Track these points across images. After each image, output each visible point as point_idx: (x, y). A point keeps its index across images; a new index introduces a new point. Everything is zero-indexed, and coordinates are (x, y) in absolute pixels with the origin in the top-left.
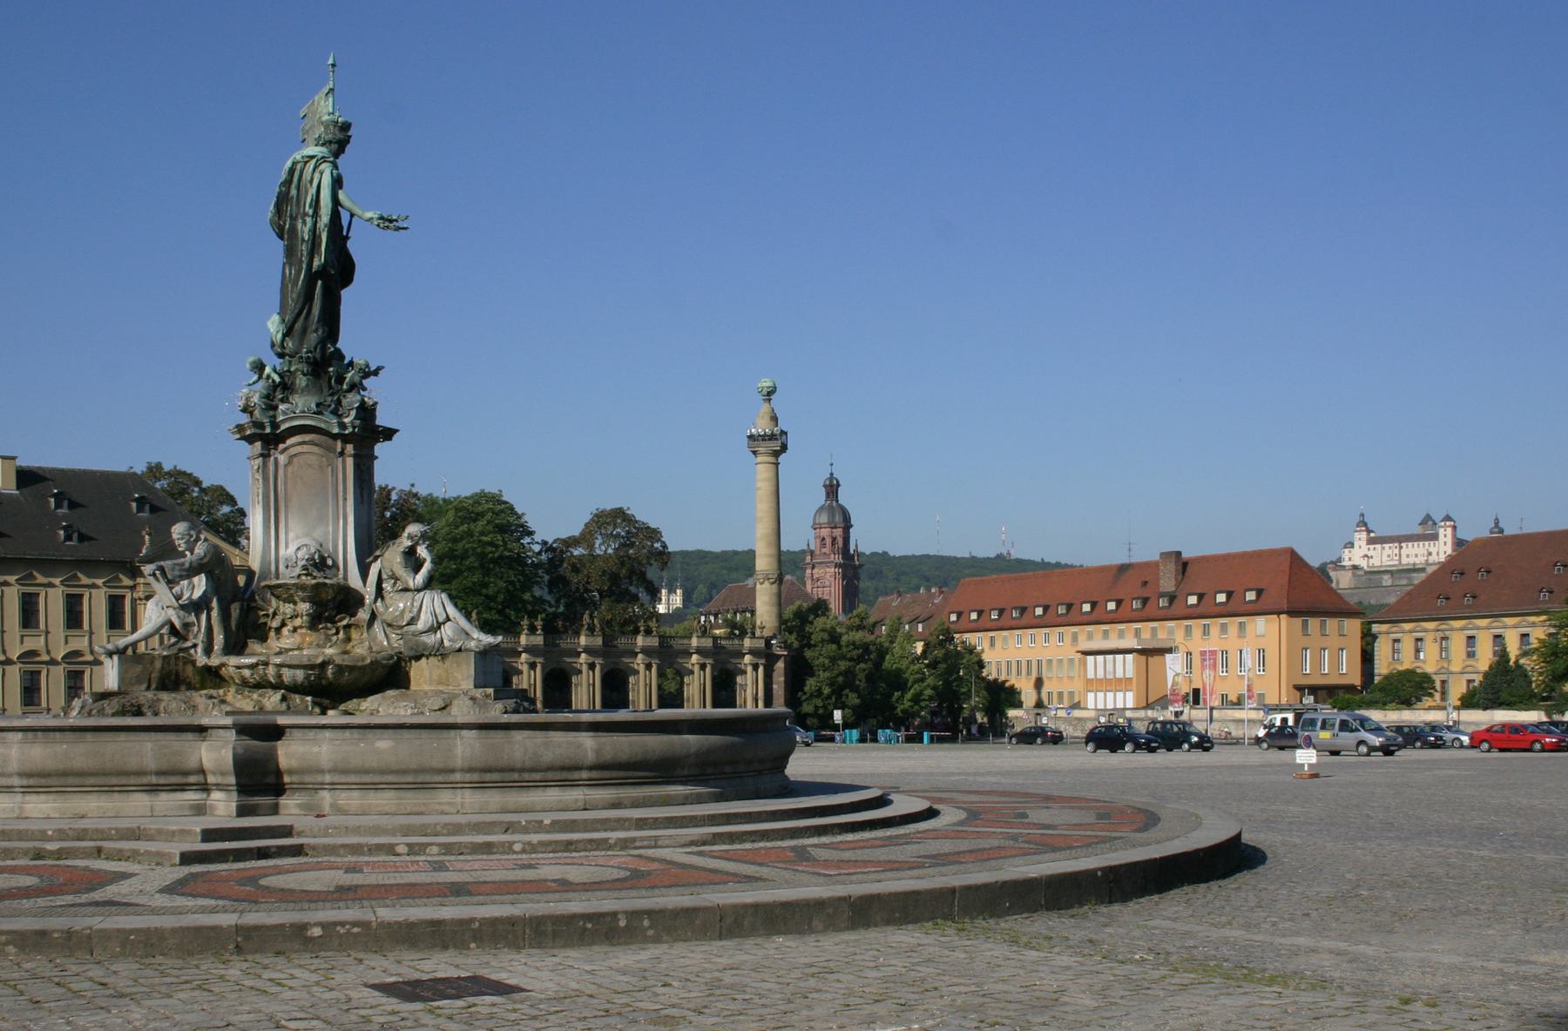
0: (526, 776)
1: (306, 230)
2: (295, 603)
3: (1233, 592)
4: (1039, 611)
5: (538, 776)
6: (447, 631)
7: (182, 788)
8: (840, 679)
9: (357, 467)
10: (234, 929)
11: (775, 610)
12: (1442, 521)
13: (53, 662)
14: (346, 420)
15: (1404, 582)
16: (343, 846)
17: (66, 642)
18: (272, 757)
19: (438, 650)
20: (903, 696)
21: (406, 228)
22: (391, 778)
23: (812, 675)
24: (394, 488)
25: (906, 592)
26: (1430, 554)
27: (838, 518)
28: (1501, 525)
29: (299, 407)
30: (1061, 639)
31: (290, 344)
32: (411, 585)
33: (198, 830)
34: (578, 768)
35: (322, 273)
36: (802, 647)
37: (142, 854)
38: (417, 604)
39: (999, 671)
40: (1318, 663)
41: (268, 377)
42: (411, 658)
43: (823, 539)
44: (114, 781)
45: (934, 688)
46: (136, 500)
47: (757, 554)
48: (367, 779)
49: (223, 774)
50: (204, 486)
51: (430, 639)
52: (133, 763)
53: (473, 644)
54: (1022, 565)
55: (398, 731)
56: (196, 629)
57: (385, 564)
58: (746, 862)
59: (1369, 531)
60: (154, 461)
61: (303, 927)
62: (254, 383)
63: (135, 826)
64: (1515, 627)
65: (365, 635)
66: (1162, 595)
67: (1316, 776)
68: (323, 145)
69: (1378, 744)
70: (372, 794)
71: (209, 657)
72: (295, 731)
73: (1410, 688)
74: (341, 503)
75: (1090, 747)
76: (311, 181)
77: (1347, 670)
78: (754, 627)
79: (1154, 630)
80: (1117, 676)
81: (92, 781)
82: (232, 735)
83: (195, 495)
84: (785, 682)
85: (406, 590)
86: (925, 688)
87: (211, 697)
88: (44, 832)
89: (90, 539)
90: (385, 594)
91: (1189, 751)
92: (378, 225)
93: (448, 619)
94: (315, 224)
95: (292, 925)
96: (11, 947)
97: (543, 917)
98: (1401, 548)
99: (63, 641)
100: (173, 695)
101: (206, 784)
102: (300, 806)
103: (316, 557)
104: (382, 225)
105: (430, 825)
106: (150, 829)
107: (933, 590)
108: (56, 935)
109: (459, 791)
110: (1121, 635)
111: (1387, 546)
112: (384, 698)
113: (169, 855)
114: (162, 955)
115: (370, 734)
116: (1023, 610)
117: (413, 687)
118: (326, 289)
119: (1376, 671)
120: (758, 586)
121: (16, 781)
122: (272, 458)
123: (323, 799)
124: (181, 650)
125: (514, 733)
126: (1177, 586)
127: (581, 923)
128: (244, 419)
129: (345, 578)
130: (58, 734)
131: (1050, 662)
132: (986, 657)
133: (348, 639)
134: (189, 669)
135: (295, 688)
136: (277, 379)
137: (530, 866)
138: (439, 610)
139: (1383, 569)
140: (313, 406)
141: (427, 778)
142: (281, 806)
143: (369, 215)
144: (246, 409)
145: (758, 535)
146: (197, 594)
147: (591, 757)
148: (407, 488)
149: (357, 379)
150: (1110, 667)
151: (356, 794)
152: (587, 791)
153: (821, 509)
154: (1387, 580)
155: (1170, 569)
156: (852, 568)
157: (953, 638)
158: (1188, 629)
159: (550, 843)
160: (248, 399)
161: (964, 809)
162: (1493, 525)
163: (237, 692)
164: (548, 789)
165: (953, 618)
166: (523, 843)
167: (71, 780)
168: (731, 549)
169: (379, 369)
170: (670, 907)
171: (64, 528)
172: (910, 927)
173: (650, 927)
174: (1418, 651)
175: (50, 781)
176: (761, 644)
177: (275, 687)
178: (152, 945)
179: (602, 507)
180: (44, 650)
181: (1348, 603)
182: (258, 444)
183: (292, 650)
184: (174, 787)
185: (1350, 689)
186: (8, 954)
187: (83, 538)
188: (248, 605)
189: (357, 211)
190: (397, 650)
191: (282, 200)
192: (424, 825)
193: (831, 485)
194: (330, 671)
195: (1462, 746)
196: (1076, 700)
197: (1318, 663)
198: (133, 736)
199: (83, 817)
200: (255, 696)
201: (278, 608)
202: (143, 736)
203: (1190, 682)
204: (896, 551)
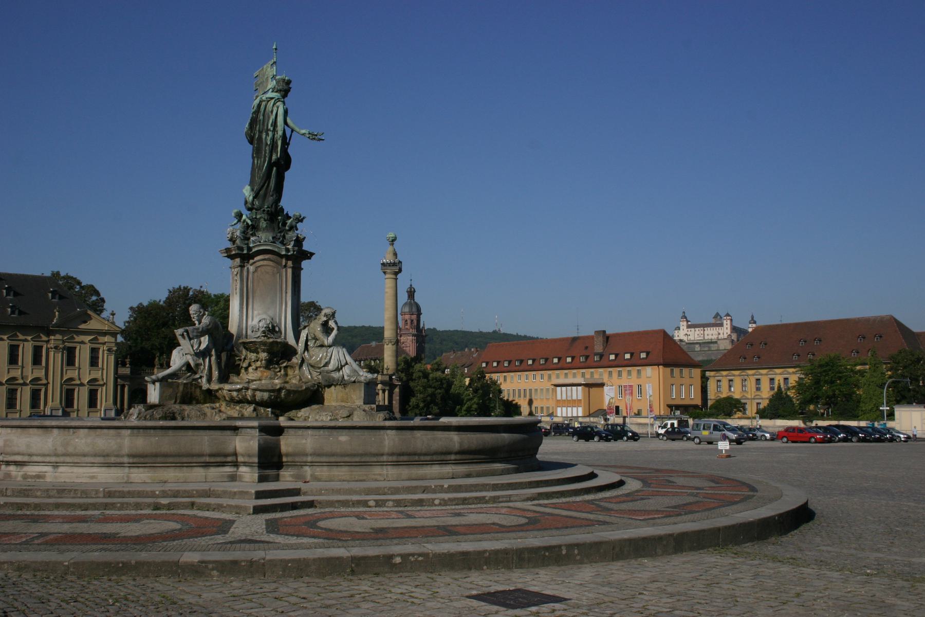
0: (422, 458)
1: (269, 138)
2: (258, 353)
3: (649, 352)
4: (530, 362)
5: (428, 458)
6: (346, 371)
7: (223, 464)
8: (429, 398)
9: (293, 273)
10: (350, 559)
11: (394, 359)
13: (82, 385)
14: (290, 247)
15: (706, 349)
16: (338, 501)
17: (8, 372)
18: (278, 446)
19: (342, 382)
20: (461, 409)
21: (323, 140)
22: (347, 459)
23: (414, 396)
24: (191, 288)
25: (458, 351)
26: (719, 334)
27: (414, 309)
28: (755, 319)
29: (262, 239)
30: (542, 377)
31: (257, 203)
32: (326, 343)
33: (253, 491)
34: (449, 453)
35: (277, 163)
36: (408, 381)
37: (225, 507)
38: (329, 355)
39: (509, 395)
40: (679, 392)
41: (244, 221)
42: (325, 386)
43: (406, 321)
44: (185, 460)
45: (478, 404)
46: (51, 292)
47: (385, 328)
48: (332, 459)
49: (249, 456)
50: (83, 285)
51: (336, 375)
52: (196, 449)
53: (362, 379)
54: (507, 337)
55: (351, 430)
56: (202, 367)
57: (311, 331)
58: (584, 512)
59: (688, 321)
60: (56, 270)
61: (391, 557)
62: (235, 224)
63: (207, 488)
64: (780, 374)
65: (297, 372)
66: (596, 354)
67: (729, 456)
68: (276, 92)
69: (734, 438)
70: (335, 469)
71: (210, 384)
72: (290, 430)
73: (731, 406)
74: (284, 294)
75: (575, 438)
76: (272, 112)
77: (694, 397)
78: (383, 369)
79: (592, 373)
81: (171, 460)
82: (256, 433)
83: (77, 290)
84: (400, 399)
85: (322, 346)
86: (473, 404)
87: (213, 408)
88: (153, 492)
89: (25, 313)
90: (310, 349)
91: (627, 441)
92: (309, 138)
93: (347, 364)
94: (274, 135)
95: (384, 556)
96: (215, 572)
97: (523, 548)
98: (704, 330)
99: (6, 372)
100: (191, 407)
101: (237, 462)
102: (292, 476)
103: (270, 326)
104: (311, 138)
105: (381, 488)
106: (218, 491)
107: (473, 350)
108: (243, 564)
109: (384, 467)
110: (574, 376)
111: (697, 329)
112: (311, 409)
113: (245, 508)
114: (307, 576)
115: (335, 432)
116: (521, 361)
117: (326, 403)
118: (278, 171)
119: (709, 397)
120: (385, 346)
121: (126, 460)
122: (246, 268)
123: (306, 471)
124: (194, 380)
125: (415, 432)
126: (604, 349)
127: (543, 553)
128: (229, 245)
129: (285, 338)
130: (152, 431)
131: (536, 390)
132: (503, 387)
133: (286, 375)
134: (198, 391)
135: (263, 404)
136: (250, 223)
137: (459, 515)
138: (342, 358)
140: (271, 238)
142: (281, 476)
143: (303, 131)
144: (232, 240)
145: (386, 318)
146: (203, 347)
147: (457, 447)
148: (198, 288)
149: (294, 223)
150: (569, 394)
151: (325, 469)
152: (454, 467)
153: (406, 304)
154: (697, 348)
156: (422, 336)
157: (485, 376)
159: (455, 499)
160: (233, 233)
161: (639, 479)
162: (751, 319)
163: (227, 405)
164: (433, 466)
165: (484, 365)
166: (440, 500)
167: (159, 459)
168: (353, 325)
169: (304, 218)
170: (588, 542)
171: (11, 307)
172: (701, 551)
173: (578, 554)
174: (730, 387)
175: (146, 460)
176: (387, 378)
177: (249, 403)
178: (301, 569)
179: (154, 299)
180: (77, 378)
181: (693, 360)
182: (238, 260)
183: (255, 380)
184: (218, 464)
185: (696, 407)
186: (213, 577)
187: (21, 313)
188: (230, 353)
189: (297, 129)
190: (317, 381)
191: (253, 122)
192: (377, 488)
193: (411, 291)
194: (283, 393)
195: (766, 440)
196: (551, 412)
197: (679, 392)
198: (196, 433)
200: (238, 408)
201: (246, 356)
202: (202, 432)
204: (440, 328)
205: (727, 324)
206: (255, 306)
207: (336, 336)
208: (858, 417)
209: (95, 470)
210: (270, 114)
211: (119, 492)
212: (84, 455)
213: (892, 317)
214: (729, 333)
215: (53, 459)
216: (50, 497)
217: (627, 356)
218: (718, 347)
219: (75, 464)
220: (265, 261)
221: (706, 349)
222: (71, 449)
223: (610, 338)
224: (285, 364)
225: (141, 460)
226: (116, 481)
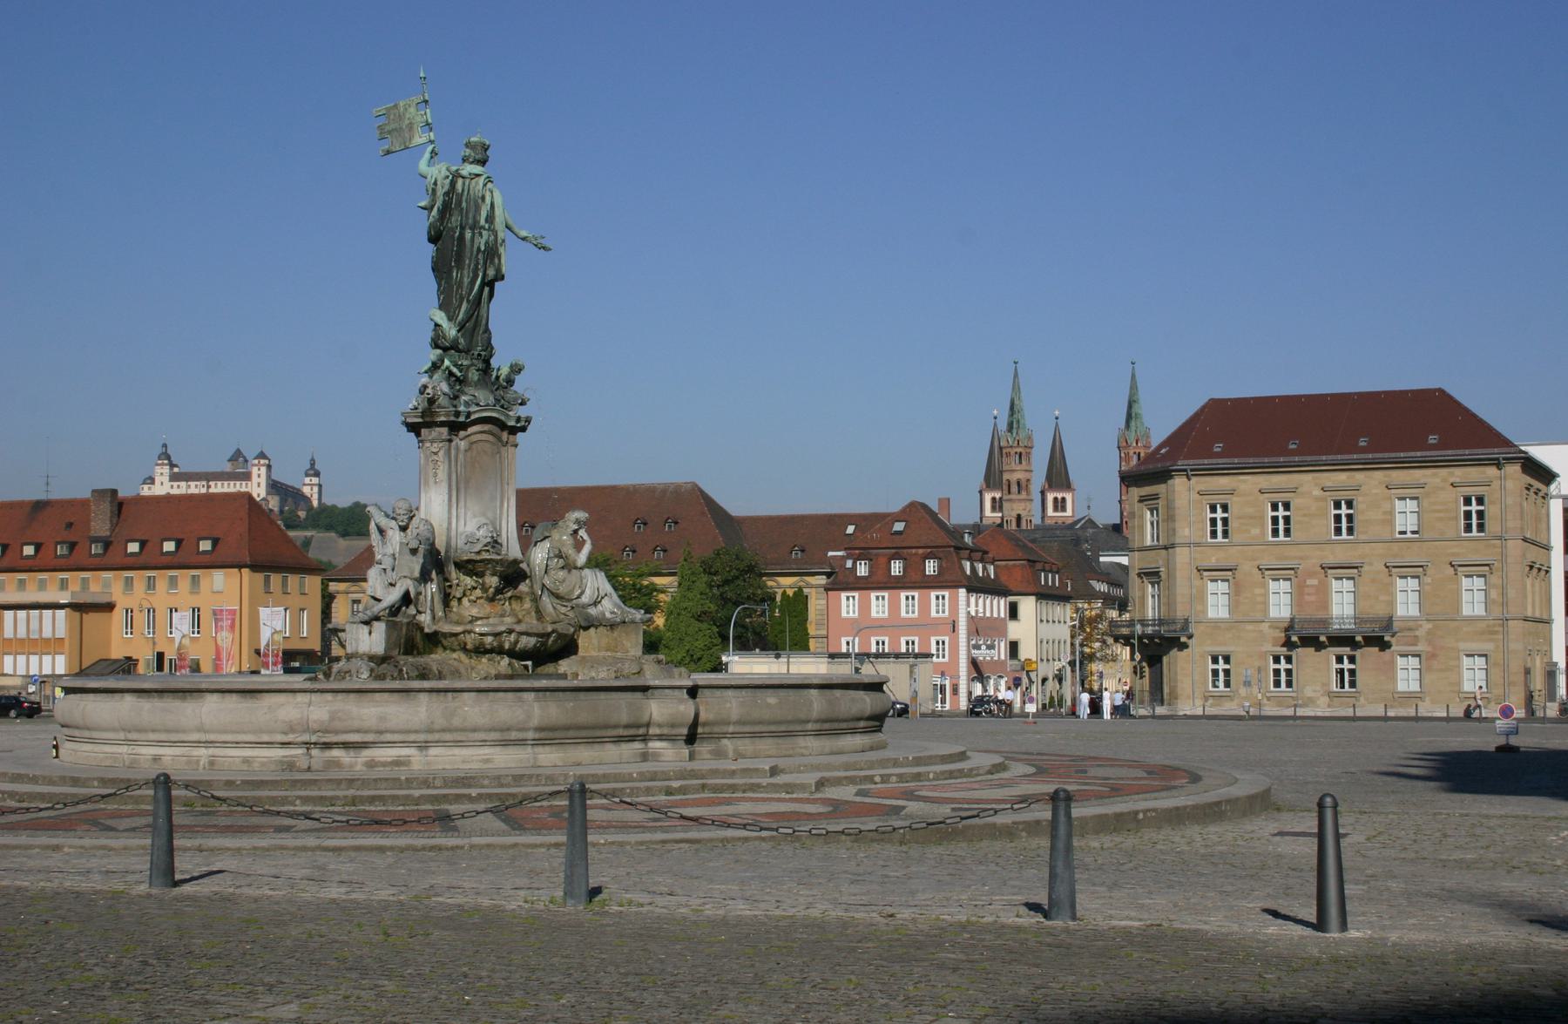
12: (255, 459)
16: (846, 778)
22: (773, 728)
41: (447, 368)
48: (757, 728)
59: (172, 465)
61: (1137, 813)
66: (96, 540)
79: (85, 581)
80: (44, 636)
88: (631, 774)
102: (710, 752)
106: (700, 770)
110: (42, 586)
126: (112, 530)
141: (791, 728)
150: (34, 625)
151: (747, 741)
155: (106, 507)
158: (129, 583)
162: (309, 466)
183: (481, 618)
199: (578, 765)
203: (154, 643)
206: (468, 504)
207: (591, 553)
209: (487, 750)
210: (480, 201)
211: (593, 775)
212: (474, 730)
213: (697, 485)
215: (422, 737)
216: (502, 786)
217: (169, 546)
219: (458, 744)
220: (484, 435)
222: (456, 722)
223: (124, 506)
224: (509, 594)
225: (550, 735)
226: (519, 765)
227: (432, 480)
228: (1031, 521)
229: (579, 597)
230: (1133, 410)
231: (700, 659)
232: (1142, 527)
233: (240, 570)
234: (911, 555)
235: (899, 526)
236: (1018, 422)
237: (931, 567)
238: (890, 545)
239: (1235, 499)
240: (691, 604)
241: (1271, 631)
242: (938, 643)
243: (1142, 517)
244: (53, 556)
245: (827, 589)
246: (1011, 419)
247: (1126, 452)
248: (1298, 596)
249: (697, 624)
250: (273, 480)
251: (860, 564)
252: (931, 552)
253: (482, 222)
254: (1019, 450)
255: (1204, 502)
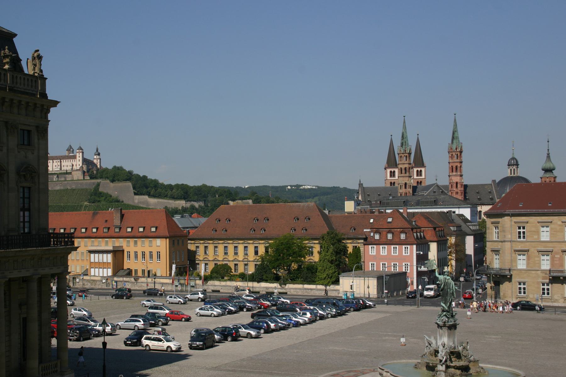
1: (451, 291)
3: (145, 227)
12: (77, 150)
66: (116, 227)
139: (53, 172)
162: (96, 151)
205: (79, 157)
208: (315, 282)
214: (81, 165)
218: (73, 177)
221: (63, 179)
227: (444, 336)
228: (411, 185)
229: (468, 356)
230: (455, 135)
231: (331, 277)
232: (492, 233)
233: (166, 239)
234: (395, 231)
235: (390, 220)
236: (405, 142)
237: (403, 236)
238: (387, 227)
239: (528, 224)
240: (328, 257)
241: (542, 274)
242: (372, 264)
243: (492, 229)
244: (407, 234)
245: (364, 245)
246: (402, 141)
247: (452, 154)
248: (552, 260)
249: (330, 264)
250: (84, 158)
251: (376, 234)
252: (402, 230)
253: (451, 288)
254: (406, 155)
255: (516, 226)
